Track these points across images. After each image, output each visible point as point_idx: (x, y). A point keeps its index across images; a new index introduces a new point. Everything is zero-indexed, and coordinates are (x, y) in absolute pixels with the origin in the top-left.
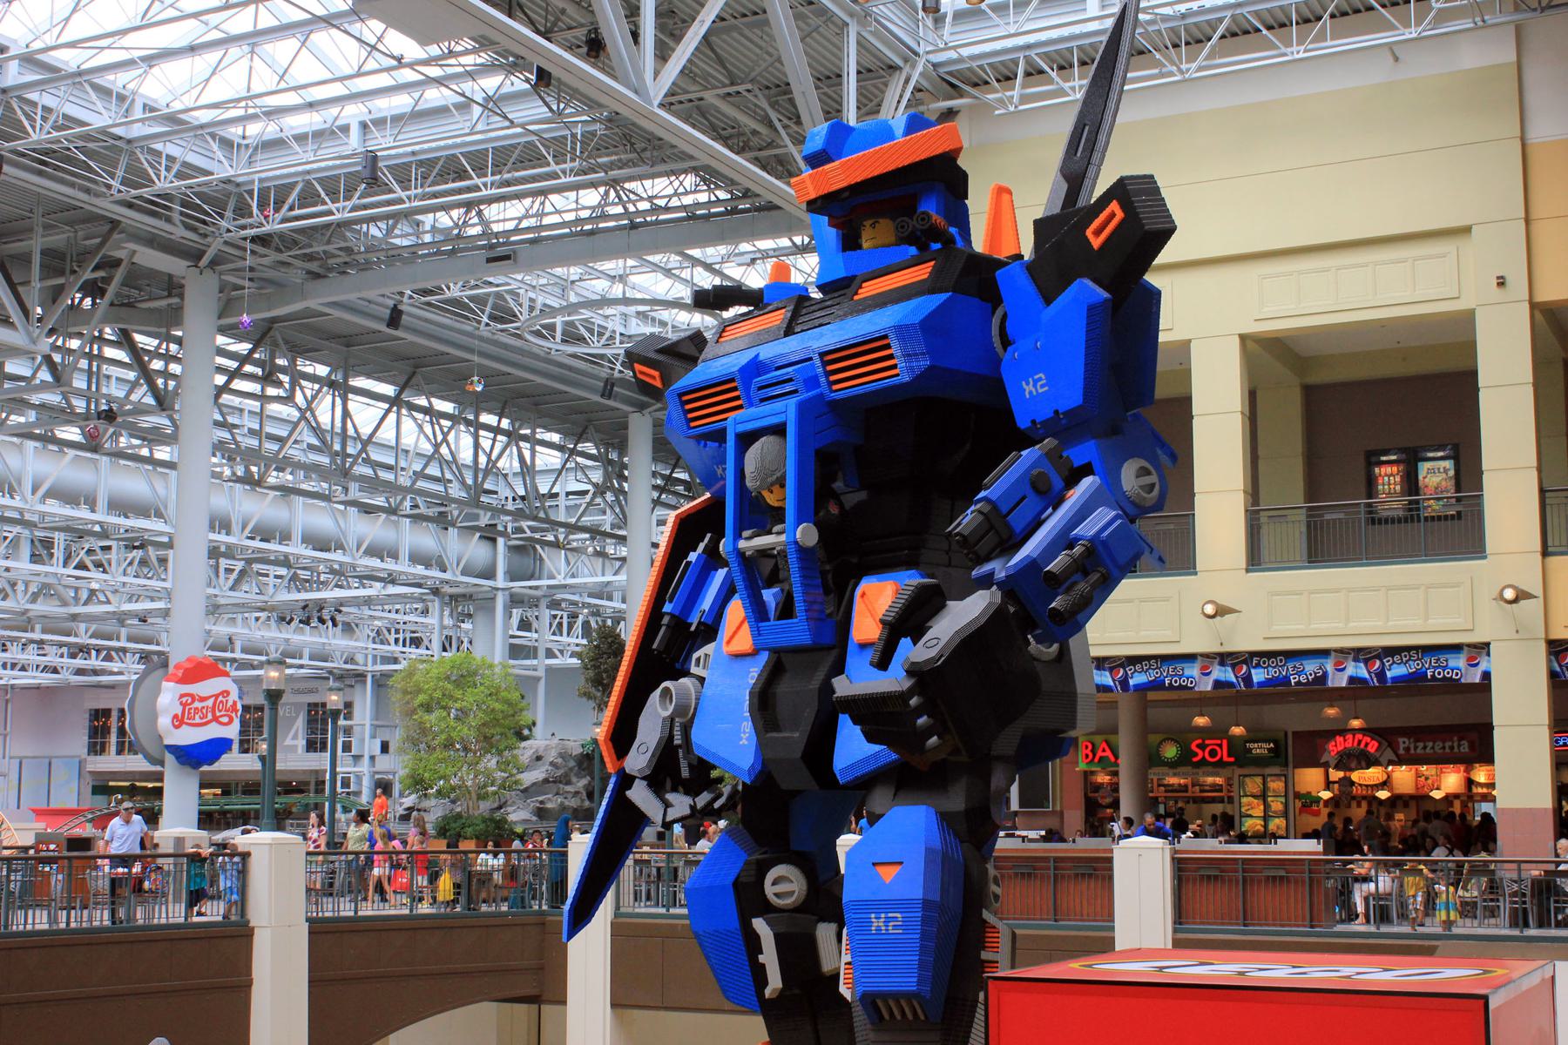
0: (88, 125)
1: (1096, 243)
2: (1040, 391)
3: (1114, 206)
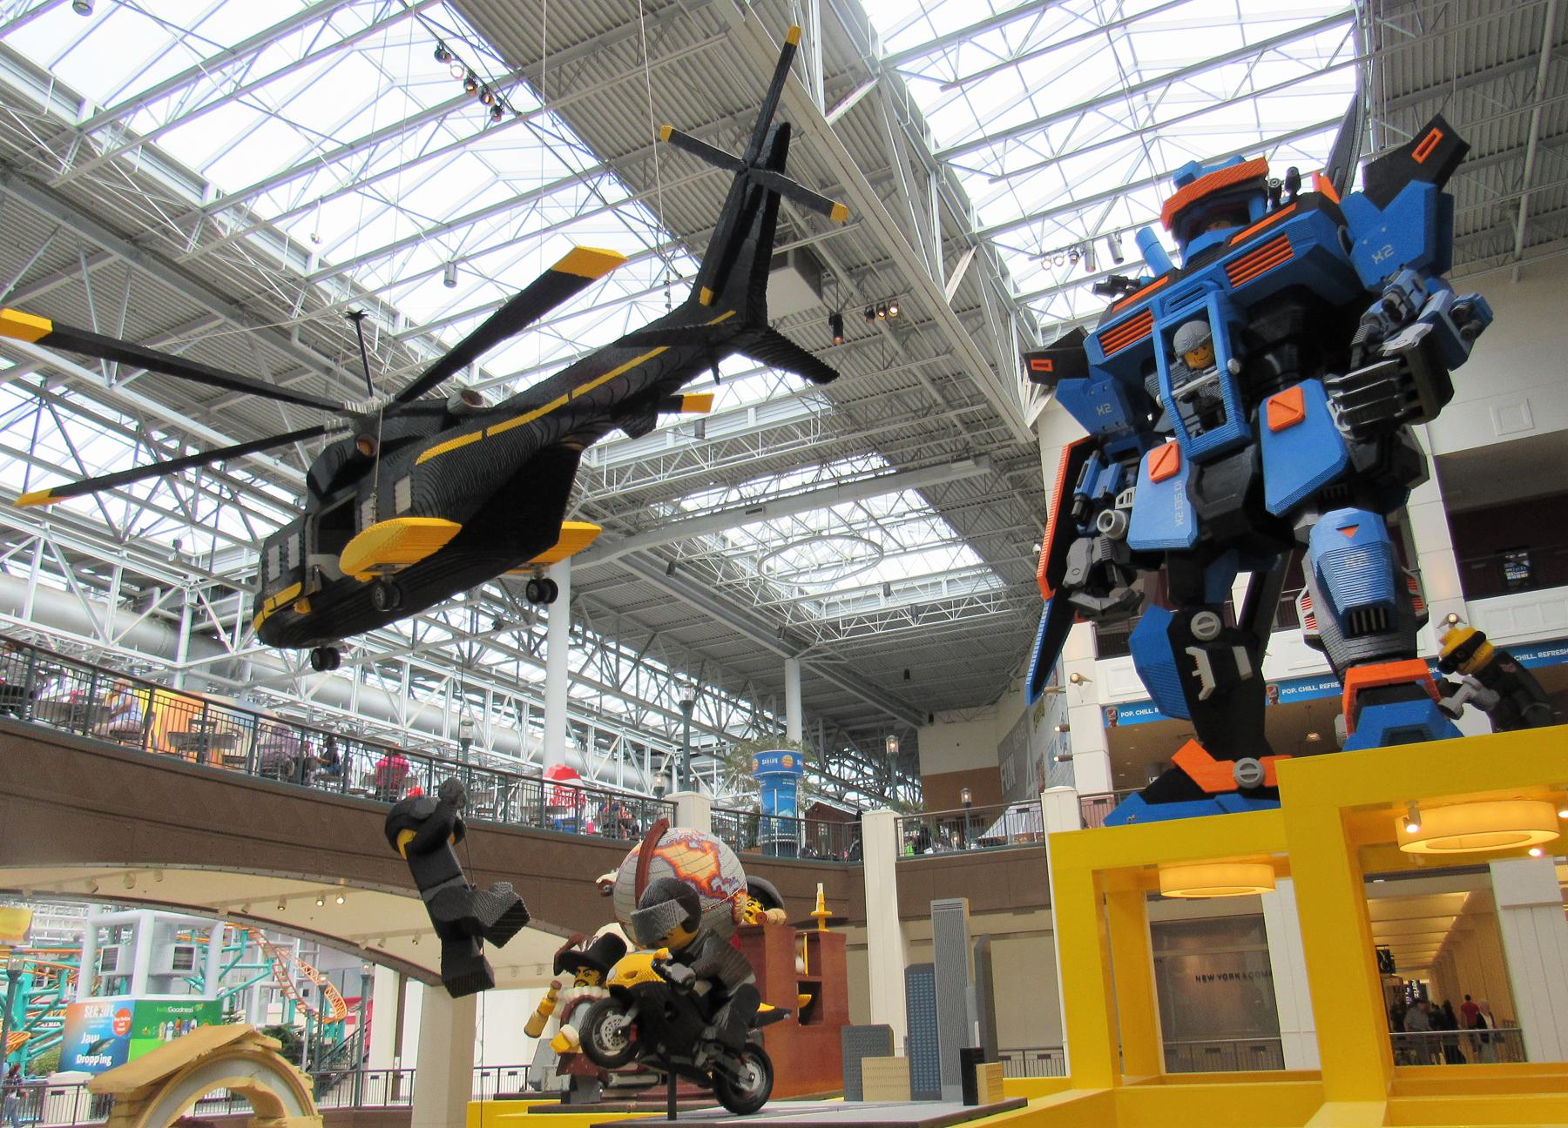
1: (1420, 160)
3: (1435, 131)
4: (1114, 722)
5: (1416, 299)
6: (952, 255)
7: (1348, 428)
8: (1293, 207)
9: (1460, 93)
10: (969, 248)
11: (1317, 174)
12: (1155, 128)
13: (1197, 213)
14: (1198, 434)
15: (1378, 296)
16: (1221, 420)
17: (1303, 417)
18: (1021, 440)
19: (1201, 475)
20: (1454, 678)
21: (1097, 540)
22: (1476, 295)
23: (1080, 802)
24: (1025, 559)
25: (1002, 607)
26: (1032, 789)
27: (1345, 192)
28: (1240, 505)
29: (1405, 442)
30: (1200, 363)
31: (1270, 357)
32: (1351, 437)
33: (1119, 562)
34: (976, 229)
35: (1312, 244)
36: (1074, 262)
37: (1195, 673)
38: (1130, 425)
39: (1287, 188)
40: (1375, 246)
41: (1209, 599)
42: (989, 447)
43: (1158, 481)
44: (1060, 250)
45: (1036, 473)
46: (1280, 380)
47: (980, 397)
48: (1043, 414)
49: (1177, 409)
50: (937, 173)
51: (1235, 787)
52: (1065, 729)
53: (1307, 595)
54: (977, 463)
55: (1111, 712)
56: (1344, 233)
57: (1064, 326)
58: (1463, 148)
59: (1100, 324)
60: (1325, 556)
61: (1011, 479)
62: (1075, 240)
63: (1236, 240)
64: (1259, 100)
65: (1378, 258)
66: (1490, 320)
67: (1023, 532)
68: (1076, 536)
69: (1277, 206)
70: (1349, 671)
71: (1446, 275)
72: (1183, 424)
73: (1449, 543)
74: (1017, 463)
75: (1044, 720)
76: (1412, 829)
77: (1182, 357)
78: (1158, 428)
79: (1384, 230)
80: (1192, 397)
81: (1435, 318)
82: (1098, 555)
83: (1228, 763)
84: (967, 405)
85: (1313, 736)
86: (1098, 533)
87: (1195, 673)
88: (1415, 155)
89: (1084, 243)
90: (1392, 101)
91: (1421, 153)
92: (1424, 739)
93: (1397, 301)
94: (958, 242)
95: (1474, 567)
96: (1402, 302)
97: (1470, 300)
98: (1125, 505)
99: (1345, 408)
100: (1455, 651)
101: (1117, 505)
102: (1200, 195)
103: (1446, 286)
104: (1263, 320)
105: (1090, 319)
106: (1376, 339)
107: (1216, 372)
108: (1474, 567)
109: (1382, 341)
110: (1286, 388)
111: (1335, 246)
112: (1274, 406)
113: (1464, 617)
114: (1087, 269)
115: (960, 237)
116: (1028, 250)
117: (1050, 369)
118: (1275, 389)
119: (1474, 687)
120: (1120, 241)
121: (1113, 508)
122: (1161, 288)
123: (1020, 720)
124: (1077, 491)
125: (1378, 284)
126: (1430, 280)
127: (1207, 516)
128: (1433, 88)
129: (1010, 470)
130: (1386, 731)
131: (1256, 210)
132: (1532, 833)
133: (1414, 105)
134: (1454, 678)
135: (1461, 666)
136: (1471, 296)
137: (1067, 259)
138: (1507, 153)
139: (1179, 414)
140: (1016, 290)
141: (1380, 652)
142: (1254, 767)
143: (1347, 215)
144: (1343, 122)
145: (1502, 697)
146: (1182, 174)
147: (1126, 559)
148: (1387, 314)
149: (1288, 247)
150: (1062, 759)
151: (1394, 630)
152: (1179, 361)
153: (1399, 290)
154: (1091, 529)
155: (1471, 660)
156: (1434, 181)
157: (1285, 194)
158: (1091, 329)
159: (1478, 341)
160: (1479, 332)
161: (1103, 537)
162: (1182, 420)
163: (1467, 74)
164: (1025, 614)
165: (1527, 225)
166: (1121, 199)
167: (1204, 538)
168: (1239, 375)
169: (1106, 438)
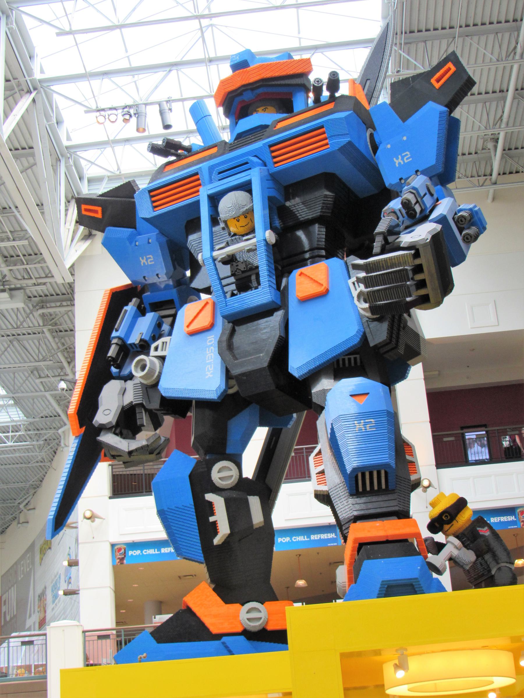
0: (4, 123)
1: (437, 85)
2: (150, 263)
3: (450, 65)
4: (122, 560)
5: (428, 201)
6: (12, 95)
7: (367, 305)
8: (331, 106)
9: (461, 39)
10: (29, 92)
11: (353, 82)
12: (211, 16)
13: (248, 96)
14: (233, 295)
15: (397, 195)
16: (254, 284)
17: (327, 291)
18: (60, 281)
19: (233, 332)
20: (440, 537)
21: (130, 384)
22: (475, 206)
23: (85, 637)
24: (47, 394)
25: (20, 439)
26: (33, 620)
27: (373, 101)
28: (265, 364)
29: (409, 324)
30: (242, 231)
31: (300, 234)
32: (369, 314)
33: (149, 407)
34: (38, 76)
35: (345, 140)
36: (126, 121)
37: (212, 519)
38: (170, 277)
39: (328, 89)
40: (397, 151)
41: (229, 450)
42: (24, 283)
43: (192, 334)
44: (115, 109)
45: (67, 313)
46: (307, 255)
47: (22, 233)
48: (81, 258)
49: (216, 269)
50: (8, 17)
51: (240, 629)
52: (73, 563)
53: (320, 453)
54: (11, 297)
55: (120, 549)
56: (372, 135)
57: (110, 179)
58: (470, 83)
59: (152, 181)
60: (339, 418)
61: (43, 316)
62: (130, 102)
63: (280, 125)
64: (301, 11)
65: (398, 161)
66: (485, 229)
67: (48, 368)
68: (110, 377)
69: (317, 100)
70: (353, 526)
71: (450, 186)
72: (221, 283)
73: (428, 419)
74: (47, 302)
75: (50, 553)
76: (401, 674)
77: (225, 222)
78: (195, 284)
79: (405, 138)
80: (230, 260)
81: (442, 220)
82: (129, 398)
83: (237, 606)
84: (8, 239)
85: (301, 583)
86: (130, 377)
87: (212, 519)
88: (433, 81)
89: (137, 106)
90: (408, 35)
91: (438, 81)
92: (415, 593)
93: (413, 201)
94: (19, 85)
95: (445, 439)
96: (417, 202)
97: (471, 210)
98: (159, 353)
99: (366, 287)
100: (444, 513)
101: (152, 352)
102: (252, 80)
103: (451, 195)
104: (297, 200)
105: (141, 175)
106: (393, 231)
107: (254, 240)
108: (445, 439)
109: (398, 233)
110: (312, 263)
111: (365, 147)
112: (302, 279)
113: (435, 483)
114: (138, 130)
115: (22, 80)
116: (85, 103)
117: (99, 216)
118: (303, 263)
119: (456, 547)
120: (170, 110)
121: (148, 354)
122: (211, 157)
123: (27, 551)
124: (114, 334)
125: (397, 184)
126: (439, 187)
127: (235, 372)
128: (440, 32)
129: (42, 307)
130: (383, 583)
131: (298, 103)
132: (495, 679)
133: (425, 42)
134: (440, 537)
135: (446, 527)
136: (471, 206)
137: (121, 118)
138: (491, 95)
139: (218, 274)
140: (69, 139)
141: (362, 513)
142: (259, 611)
143: (375, 119)
144: (375, 43)
145: (478, 556)
146: (238, 60)
147: (155, 405)
148: (404, 211)
149: (326, 139)
150: (66, 593)
151: (393, 491)
152: (222, 225)
153: (415, 191)
154: (125, 372)
155: (454, 522)
156: (446, 106)
157: (326, 93)
158: (143, 184)
159: (473, 245)
160: (475, 238)
161: (137, 381)
162: (220, 279)
163: (467, 26)
164: (41, 448)
165: (502, 157)
166: (174, 72)
167: (231, 391)
168: (274, 246)
169: (144, 289)
